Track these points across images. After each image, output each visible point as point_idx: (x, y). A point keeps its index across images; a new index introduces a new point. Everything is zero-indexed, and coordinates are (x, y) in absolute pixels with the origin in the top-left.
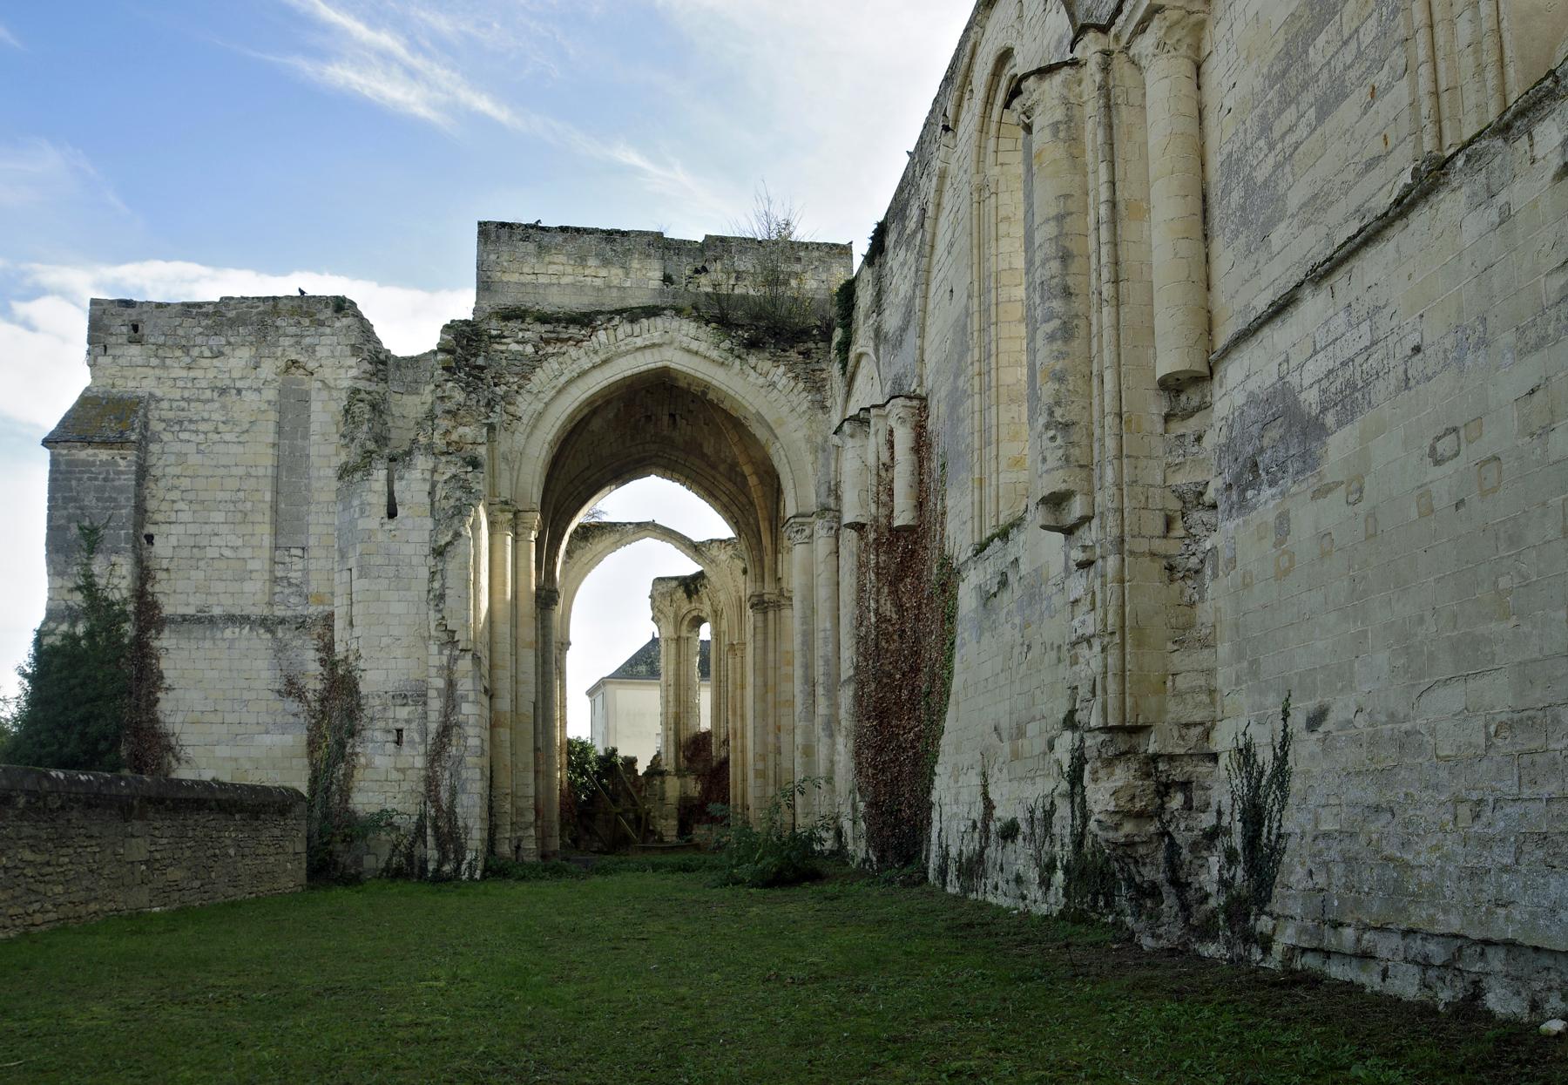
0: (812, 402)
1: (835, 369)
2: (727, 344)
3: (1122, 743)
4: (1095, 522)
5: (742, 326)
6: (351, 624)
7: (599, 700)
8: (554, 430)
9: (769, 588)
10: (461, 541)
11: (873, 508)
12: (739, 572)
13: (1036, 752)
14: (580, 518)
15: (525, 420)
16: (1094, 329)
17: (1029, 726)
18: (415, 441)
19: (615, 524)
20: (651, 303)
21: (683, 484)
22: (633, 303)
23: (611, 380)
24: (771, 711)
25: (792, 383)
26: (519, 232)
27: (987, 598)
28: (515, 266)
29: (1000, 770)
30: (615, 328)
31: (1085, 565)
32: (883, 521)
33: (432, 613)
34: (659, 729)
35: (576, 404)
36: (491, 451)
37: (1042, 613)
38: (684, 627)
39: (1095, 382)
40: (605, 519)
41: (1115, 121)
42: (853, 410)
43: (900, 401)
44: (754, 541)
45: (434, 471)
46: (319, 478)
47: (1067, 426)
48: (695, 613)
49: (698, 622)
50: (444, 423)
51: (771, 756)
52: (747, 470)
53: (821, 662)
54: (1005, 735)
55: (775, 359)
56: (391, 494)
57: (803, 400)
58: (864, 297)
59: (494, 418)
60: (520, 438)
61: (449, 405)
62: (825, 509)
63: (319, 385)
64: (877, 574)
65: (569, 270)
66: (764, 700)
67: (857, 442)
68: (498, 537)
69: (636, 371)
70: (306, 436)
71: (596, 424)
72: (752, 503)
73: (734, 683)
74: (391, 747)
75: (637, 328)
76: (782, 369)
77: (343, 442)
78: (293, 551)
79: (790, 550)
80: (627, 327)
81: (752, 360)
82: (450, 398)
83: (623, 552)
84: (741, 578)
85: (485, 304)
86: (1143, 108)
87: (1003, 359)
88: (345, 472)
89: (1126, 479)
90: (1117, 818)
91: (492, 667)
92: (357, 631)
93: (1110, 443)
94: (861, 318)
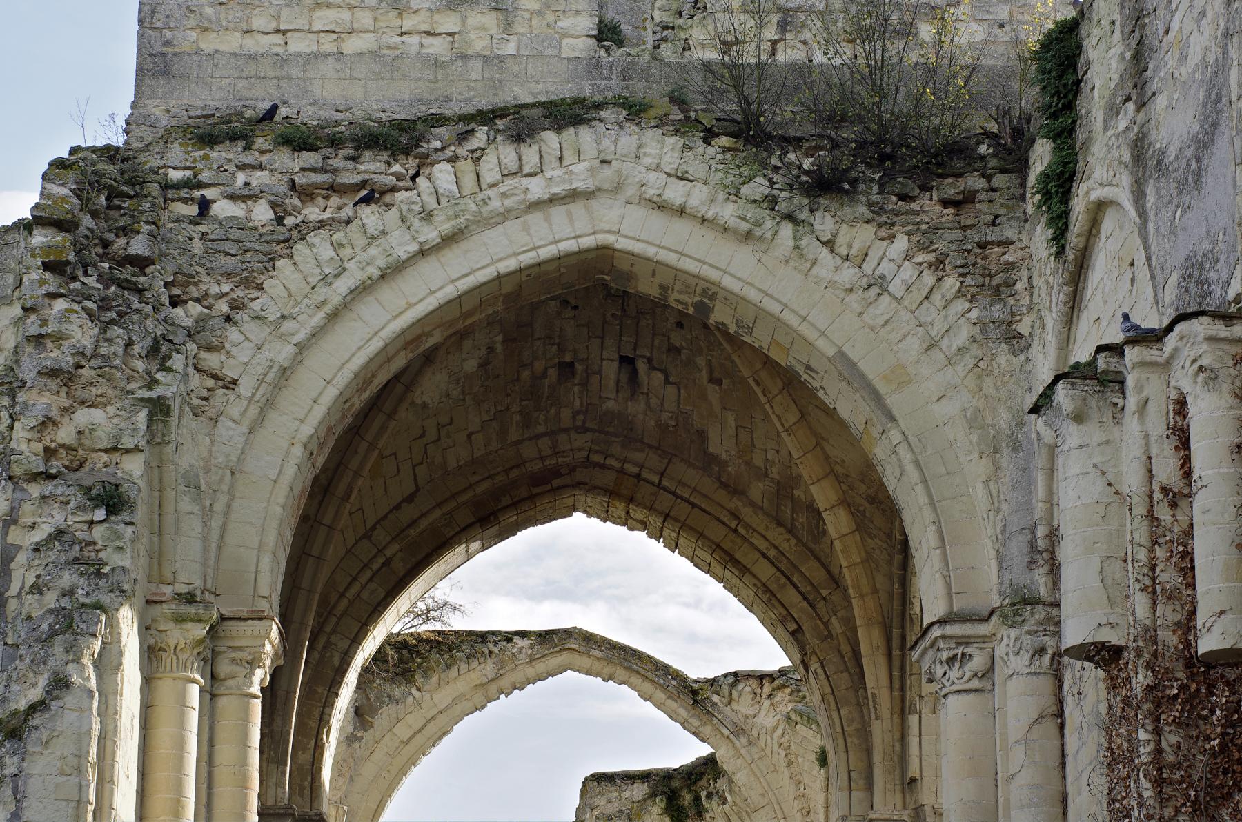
0: (982, 324)
2: (758, 188)
5: (796, 142)
8: (319, 412)
10: (69, 700)
11: (1141, 604)
12: (808, 761)
14: (394, 621)
15: (245, 388)
19: (483, 637)
20: (566, 91)
21: (657, 535)
22: (523, 94)
23: (465, 284)
25: (929, 279)
28: (232, 14)
30: (477, 156)
32: (1170, 639)
35: (376, 345)
36: (156, 469)
40: (457, 623)
42: (1082, 353)
43: (1200, 327)
44: (843, 680)
50: (40, 401)
52: (823, 495)
55: (883, 220)
57: (957, 320)
58: (1104, 62)
59: (168, 386)
60: (231, 433)
61: (55, 356)
62: (1024, 601)
64: (1159, 783)
65: (365, 19)
67: (1093, 432)
68: (165, 687)
69: (528, 259)
71: (432, 388)
72: (836, 581)
75: (530, 154)
76: (902, 243)
79: (939, 699)
80: (507, 153)
81: (824, 224)
82: (58, 338)
84: (815, 778)
85: (155, 109)
94: (1098, 125)
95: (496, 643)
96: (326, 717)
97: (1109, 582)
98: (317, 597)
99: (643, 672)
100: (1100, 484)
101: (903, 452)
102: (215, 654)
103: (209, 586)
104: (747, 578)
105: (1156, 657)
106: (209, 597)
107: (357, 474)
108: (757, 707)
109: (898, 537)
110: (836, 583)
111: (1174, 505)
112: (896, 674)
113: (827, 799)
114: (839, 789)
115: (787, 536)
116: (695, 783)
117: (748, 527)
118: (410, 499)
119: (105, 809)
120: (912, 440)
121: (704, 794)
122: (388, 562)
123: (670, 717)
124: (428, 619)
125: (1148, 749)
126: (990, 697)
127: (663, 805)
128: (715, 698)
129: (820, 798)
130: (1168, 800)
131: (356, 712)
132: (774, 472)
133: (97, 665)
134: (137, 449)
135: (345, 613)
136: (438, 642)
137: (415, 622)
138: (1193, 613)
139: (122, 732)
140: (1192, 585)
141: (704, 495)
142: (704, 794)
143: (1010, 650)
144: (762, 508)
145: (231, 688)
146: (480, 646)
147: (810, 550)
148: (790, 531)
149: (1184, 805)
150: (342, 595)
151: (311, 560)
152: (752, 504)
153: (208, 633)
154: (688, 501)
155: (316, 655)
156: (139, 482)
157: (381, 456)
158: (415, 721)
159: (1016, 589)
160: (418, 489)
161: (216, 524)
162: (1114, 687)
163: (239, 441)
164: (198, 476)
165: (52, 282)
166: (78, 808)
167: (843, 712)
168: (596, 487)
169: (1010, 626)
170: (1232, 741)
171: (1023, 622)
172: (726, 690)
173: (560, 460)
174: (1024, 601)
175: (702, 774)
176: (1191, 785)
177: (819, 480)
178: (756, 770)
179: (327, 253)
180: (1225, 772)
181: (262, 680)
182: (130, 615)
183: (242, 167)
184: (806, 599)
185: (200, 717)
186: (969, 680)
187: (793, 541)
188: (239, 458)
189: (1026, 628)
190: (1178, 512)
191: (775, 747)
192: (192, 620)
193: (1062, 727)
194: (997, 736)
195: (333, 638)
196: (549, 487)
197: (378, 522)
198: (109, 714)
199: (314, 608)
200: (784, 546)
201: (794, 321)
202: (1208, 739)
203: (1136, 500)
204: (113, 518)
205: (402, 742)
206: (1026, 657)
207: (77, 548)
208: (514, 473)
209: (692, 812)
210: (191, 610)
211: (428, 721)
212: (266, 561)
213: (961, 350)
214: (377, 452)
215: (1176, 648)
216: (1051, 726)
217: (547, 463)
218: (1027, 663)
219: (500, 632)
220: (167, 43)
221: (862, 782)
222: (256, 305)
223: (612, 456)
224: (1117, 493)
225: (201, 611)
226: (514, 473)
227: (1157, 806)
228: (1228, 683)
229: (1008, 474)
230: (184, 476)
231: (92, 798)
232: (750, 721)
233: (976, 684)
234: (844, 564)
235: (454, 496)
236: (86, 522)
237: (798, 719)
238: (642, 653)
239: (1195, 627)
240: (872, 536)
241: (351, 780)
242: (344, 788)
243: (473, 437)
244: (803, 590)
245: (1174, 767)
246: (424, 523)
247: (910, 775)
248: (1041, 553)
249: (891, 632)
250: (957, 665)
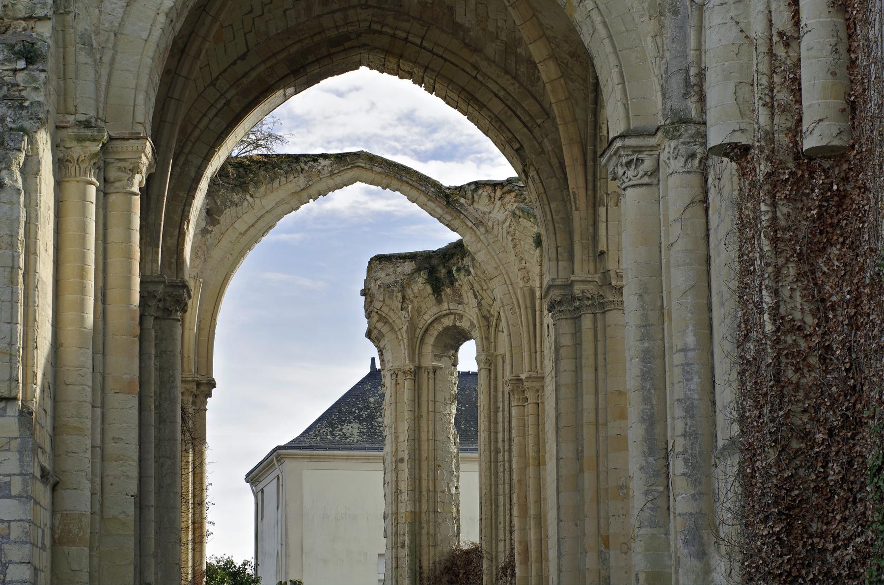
11: (763, 116)
12: (528, 243)
14: (232, 147)
19: (297, 158)
21: (419, 82)
32: (783, 139)
34: (381, 545)
36: (60, 31)
40: (279, 149)
48: (447, 322)
52: (537, 51)
53: (679, 412)
64: (775, 241)
68: (71, 188)
72: (547, 113)
73: (523, 455)
84: (533, 255)
95: (306, 163)
96: (186, 213)
97: (741, 100)
98: (178, 127)
99: (410, 182)
100: (735, 30)
102: (106, 164)
103: (101, 115)
104: (484, 112)
105: (773, 153)
106: (100, 123)
107: (205, 39)
108: (492, 206)
109: (591, 81)
110: (547, 114)
111: (787, 45)
112: (590, 178)
113: (541, 270)
114: (550, 260)
115: (512, 81)
116: (448, 261)
117: (484, 75)
118: (243, 57)
119: (31, 273)
120: (602, 7)
121: (454, 269)
122: (227, 103)
123: (431, 214)
124: (257, 146)
125: (767, 217)
126: (656, 189)
127: (426, 277)
128: (462, 200)
129: (536, 270)
130: (781, 252)
131: (207, 213)
132: (503, 36)
133: (22, 171)
134: (46, 18)
135: (198, 139)
136: (265, 163)
137: (248, 149)
138: (800, 120)
139: (41, 219)
140: (799, 102)
141: (454, 53)
142: (454, 269)
143: (671, 155)
144: (494, 62)
145: (118, 188)
146: (295, 165)
147: (530, 92)
148: (514, 78)
149: (792, 256)
150: (196, 127)
151: (173, 101)
152: (487, 59)
153: (101, 148)
154: (441, 57)
155: (178, 169)
156: (48, 41)
157: (222, 26)
158: (249, 218)
159: (674, 112)
160: (248, 50)
161: (104, 71)
162: (744, 175)
163: (119, 12)
164: (90, 37)
166: (11, 272)
167: (553, 205)
168: (375, 48)
169: (671, 139)
170: (826, 211)
171: (680, 135)
172: (469, 194)
173: (350, 28)
174: (680, 120)
175: (453, 255)
176: (797, 242)
177: (535, 41)
178: (491, 251)
180: (821, 233)
181: (140, 183)
182: (45, 136)
184: (526, 126)
185: (96, 209)
186: (642, 177)
187: (517, 85)
188: (120, 24)
189: (682, 140)
190: (790, 50)
191: (505, 235)
192: (89, 140)
193: (707, 210)
194: (661, 217)
195: (190, 158)
196: (342, 48)
197: (220, 74)
198: (32, 206)
199: (176, 135)
200: (510, 89)
202: (809, 209)
203: (760, 41)
204: (31, 67)
205: (241, 233)
206: (682, 160)
207: (5, 88)
208: (317, 38)
209: (446, 281)
210: (88, 132)
211: (259, 219)
212: (141, 97)
214: (218, 24)
215: (787, 146)
216: (699, 209)
217: (340, 30)
218: (683, 165)
219: (309, 155)
221: (566, 255)
223: (387, 25)
224: (747, 37)
225: (96, 133)
226: (317, 38)
227: (773, 257)
228: (824, 170)
229: (669, 31)
230: (81, 37)
231: (22, 265)
232: (487, 216)
233: (646, 180)
234: (553, 101)
235: (274, 55)
236: (11, 70)
237: (521, 214)
238: (410, 169)
239: (801, 131)
240: (572, 80)
241: (205, 260)
242: (200, 266)
243: (287, 12)
244: (524, 120)
245: (785, 229)
246: (253, 75)
247: (600, 249)
248: (693, 86)
249: (586, 149)
250: (633, 167)
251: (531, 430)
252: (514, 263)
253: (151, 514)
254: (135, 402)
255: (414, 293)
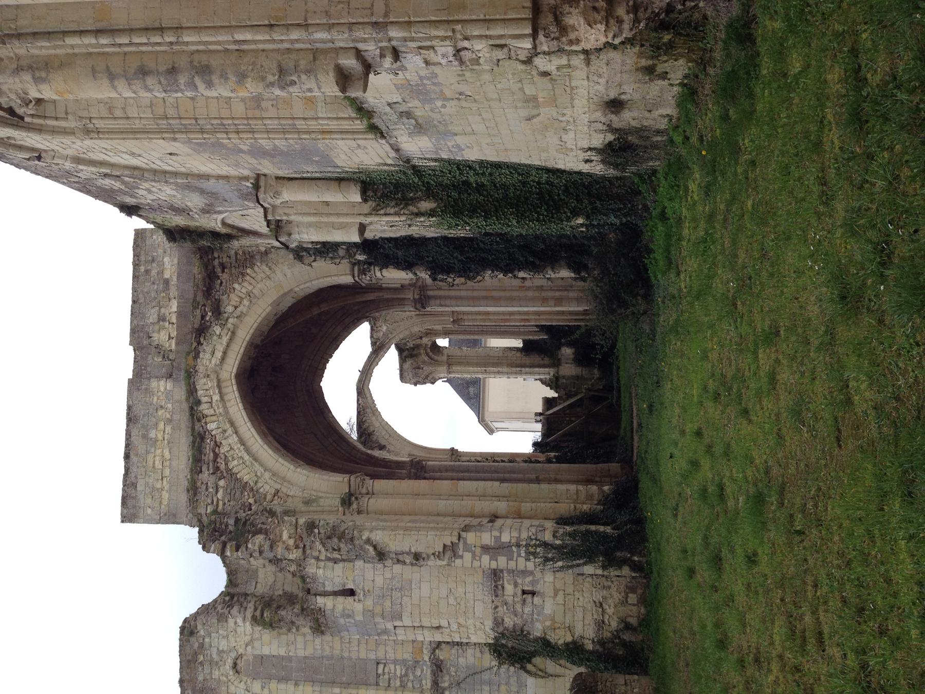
1: (236, 244)
2: (217, 330)
3: (547, 19)
4: (361, 46)
6: (438, 628)
7: (497, 425)
8: (286, 464)
9: (409, 295)
13: (550, 86)
14: (360, 446)
16: (201, 48)
17: (528, 92)
18: (294, 575)
19: (359, 413)
24: (508, 294)
25: (248, 278)
26: (131, 491)
27: (420, 128)
29: (564, 115)
31: (396, 54)
33: (430, 563)
34: (520, 379)
35: (265, 447)
37: (434, 84)
38: (439, 358)
39: (245, 47)
40: (354, 420)
41: (30, 30)
43: (261, 196)
45: (317, 559)
46: (322, 649)
47: (282, 71)
49: (435, 346)
50: (280, 551)
51: (544, 294)
54: (535, 112)
56: (336, 594)
57: (260, 269)
58: (179, 221)
61: (266, 547)
63: (249, 648)
65: (159, 452)
66: (499, 299)
69: (239, 400)
70: (290, 659)
73: (484, 320)
74: (537, 600)
75: (204, 399)
77: (294, 630)
78: (380, 671)
82: (260, 546)
83: (380, 406)
86: (18, 7)
87: (225, 113)
88: (319, 628)
89: (324, 21)
90: (612, 21)
91: (472, 516)
92: (444, 623)
93: (295, 35)
101: (302, 287)
165: (243, 548)
179: (235, 462)
183: (207, 489)
201: (260, 319)
213: (270, 268)
220: (165, 515)
222: (252, 484)
251: (474, 317)
252: (406, 321)
253: (507, 475)
254: (461, 482)
255: (419, 364)
